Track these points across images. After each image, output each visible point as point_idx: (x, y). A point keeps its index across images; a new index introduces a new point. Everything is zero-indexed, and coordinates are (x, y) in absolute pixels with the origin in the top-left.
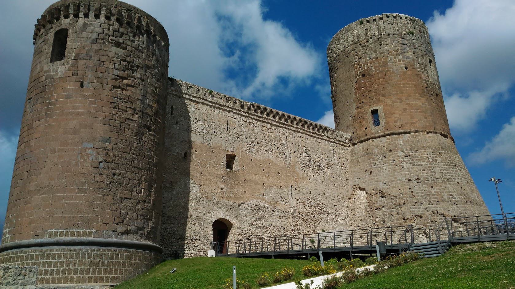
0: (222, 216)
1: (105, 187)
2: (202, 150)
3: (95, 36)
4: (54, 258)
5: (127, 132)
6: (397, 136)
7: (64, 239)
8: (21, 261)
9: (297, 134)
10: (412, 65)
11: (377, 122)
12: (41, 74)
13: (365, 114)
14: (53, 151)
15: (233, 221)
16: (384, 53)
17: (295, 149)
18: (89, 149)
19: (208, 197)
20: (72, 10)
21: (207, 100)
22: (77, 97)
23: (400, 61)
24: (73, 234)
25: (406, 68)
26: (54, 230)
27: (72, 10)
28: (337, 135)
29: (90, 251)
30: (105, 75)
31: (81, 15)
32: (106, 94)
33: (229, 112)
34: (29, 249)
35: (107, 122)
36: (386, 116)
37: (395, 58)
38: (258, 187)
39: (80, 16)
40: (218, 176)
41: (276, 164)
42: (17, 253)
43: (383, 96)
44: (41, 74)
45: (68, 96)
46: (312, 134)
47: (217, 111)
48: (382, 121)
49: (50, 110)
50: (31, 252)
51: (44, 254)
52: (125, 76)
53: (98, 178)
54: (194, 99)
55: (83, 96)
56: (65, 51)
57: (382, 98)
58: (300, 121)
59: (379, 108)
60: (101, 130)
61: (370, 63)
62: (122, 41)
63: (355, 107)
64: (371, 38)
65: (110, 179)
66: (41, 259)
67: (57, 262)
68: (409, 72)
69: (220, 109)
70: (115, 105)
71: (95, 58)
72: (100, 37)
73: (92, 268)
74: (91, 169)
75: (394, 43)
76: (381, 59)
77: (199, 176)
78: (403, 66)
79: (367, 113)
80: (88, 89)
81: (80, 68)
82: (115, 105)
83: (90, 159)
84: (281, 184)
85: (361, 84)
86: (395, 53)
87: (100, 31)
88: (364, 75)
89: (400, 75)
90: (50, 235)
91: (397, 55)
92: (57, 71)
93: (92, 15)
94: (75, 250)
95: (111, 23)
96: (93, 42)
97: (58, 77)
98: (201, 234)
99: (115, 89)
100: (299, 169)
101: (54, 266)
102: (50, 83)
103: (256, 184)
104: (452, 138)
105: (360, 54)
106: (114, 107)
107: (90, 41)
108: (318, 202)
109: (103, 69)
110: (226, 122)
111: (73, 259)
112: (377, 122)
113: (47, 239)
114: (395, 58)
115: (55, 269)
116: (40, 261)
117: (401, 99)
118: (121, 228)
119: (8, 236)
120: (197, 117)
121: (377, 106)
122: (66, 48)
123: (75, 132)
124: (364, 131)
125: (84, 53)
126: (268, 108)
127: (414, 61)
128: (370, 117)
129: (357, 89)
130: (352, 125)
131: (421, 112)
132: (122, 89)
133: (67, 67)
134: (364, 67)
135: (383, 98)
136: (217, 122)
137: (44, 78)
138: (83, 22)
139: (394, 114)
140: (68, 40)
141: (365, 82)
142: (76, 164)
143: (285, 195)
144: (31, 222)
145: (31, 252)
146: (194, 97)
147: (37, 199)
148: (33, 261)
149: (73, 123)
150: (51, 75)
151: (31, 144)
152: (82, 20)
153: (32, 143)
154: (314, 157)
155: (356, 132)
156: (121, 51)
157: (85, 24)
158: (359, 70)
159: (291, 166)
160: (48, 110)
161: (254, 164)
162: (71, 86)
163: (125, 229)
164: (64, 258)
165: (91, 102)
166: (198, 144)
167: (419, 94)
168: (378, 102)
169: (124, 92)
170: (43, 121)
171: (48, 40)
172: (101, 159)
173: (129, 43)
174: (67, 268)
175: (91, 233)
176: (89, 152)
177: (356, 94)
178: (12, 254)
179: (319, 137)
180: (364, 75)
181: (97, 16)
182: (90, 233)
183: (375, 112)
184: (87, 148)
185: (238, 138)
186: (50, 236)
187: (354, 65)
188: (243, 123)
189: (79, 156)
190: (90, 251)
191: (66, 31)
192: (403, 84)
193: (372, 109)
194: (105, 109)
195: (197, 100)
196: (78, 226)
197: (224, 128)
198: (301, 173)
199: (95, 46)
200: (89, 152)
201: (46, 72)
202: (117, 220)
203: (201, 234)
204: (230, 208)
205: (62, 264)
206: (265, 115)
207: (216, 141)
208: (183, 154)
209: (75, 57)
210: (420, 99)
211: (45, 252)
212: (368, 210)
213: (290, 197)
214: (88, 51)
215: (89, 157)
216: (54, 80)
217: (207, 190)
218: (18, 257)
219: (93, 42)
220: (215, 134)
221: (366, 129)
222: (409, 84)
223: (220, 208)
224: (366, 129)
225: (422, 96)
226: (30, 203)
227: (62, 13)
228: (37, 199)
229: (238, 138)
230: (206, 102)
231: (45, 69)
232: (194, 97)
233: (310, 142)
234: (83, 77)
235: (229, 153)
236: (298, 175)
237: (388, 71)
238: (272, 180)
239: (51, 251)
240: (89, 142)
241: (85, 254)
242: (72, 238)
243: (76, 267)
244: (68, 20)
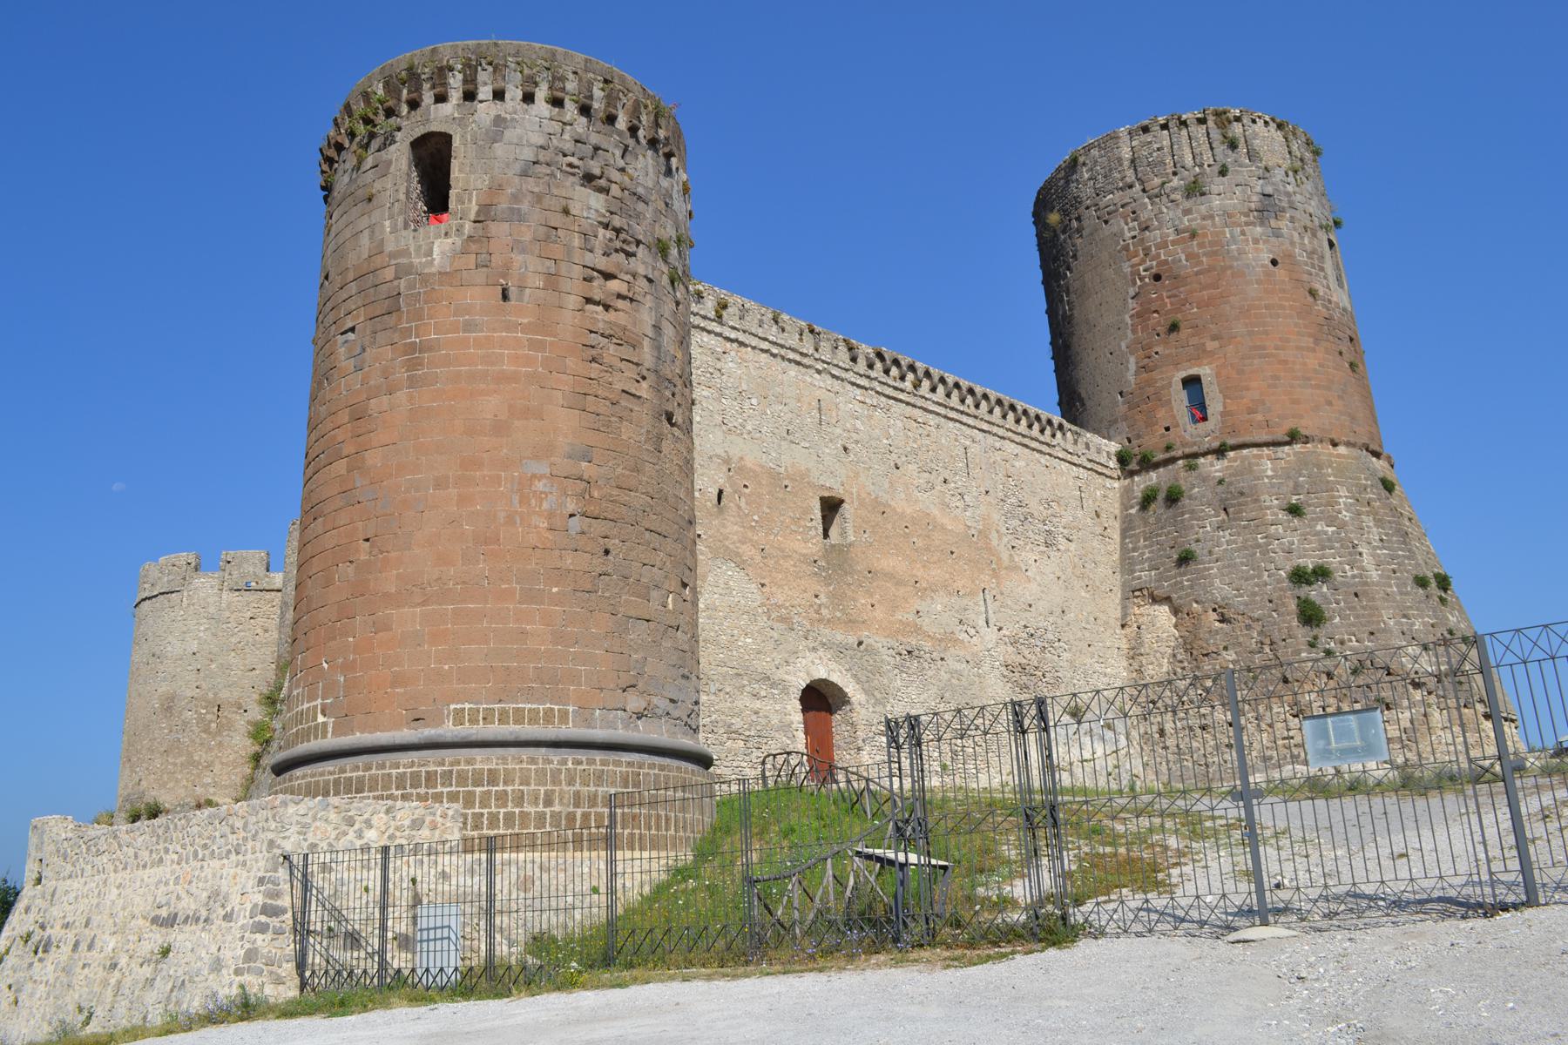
0: (821, 673)
1: (588, 587)
2: (760, 483)
3: (528, 154)
4: (478, 782)
5: (627, 432)
6: (1255, 451)
7: (495, 730)
8: (385, 788)
9: (991, 439)
10: (1290, 256)
11: (1199, 410)
12: (378, 261)
13: (1163, 388)
14: (440, 484)
15: (850, 688)
16: (1212, 217)
17: (988, 485)
18: (540, 478)
19: (782, 619)
20: (456, 82)
21: (765, 339)
22: (494, 330)
23: (1256, 241)
24: (519, 717)
25: (1274, 262)
26: (467, 706)
27: (456, 82)
28: (1088, 447)
29: (570, 765)
30: (563, 267)
31: (485, 92)
32: (570, 315)
33: (819, 372)
34: (404, 758)
35: (579, 400)
36: (1225, 397)
37: (1243, 233)
38: (902, 590)
39: (481, 96)
40: (804, 559)
41: (943, 528)
42: (368, 768)
43: (1215, 338)
44: (378, 261)
45: (469, 327)
46: (1026, 441)
47: (793, 371)
48: (1214, 406)
49: (421, 364)
50: (412, 764)
51: (451, 772)
52: (611, 270)
53: (569, 561)
54: (733, 335)
55: (510, 327)
56: (447, 197)
57: (1211, 345)
58: (999, 402)
59: (1205, 371)
60: (565, 426)
61: (1174, 243)
62: (597, 172)
63: (1132, 366)
64: (1175, 174)
65: (598, 564)
66: (443, 785)
67: (489, 792)
68: (1280, 272)
69: (798, 363)
70: (594, 352)
71: (536, 216)
72: (541, 158)
73: (579, 812)
74: (549, 535)
75: (1238, 190)
76: (1205, 235)
77: (758, 558)
78: (1266, 258)
79: (1170, 384)
80: (523, 311)
81: (494, 246)
82: (594, 352)
83: (545, 505)
84: (959, 585)
85: (1151, 301)
86: (1243, 219)
87: (539, 140)
88: (1157, 278)
89: (1259, 282)
90: (459, 717)
91: (1247, 224)
92: (430, 253)
93: (514, 93)
94: (533, 761)
95: (568, 118)
96: (524, 174)
97: (434, 270)
98: (775, 721)
99: (590, 307)
100: (1000, 544)
101: (483, 805)
102: (411, 286)
103: (900, 583)
104: (1389, 459)
105: (1144, 216)
106: (594, 360)
107: (518, 167)
108: (1050, 636)
109: (557, 251)
110: (815, 403)
111: (528, 784)
112: (1199, 410)
113: (449, 730)
114: (1243, 233)
115: (485, 811)
116: (439, 789)
117: (1264, 348)
118: (635, 702)
119: (321, 719)
120: (744, 387)
121: (1199, 366)
122: (449, 187)
123: (500, 428)
124: (1162, 436)
125: (503, 205)
126: (918, 364)
127: (1292, 243)
128: (1180, 398)
129: (1138, 315)
130: (1125, 418)
131: (1317, 387)
132: (607, 307)
133: (459, 241)
134: (1158, 255)
135: (1216, 344)
136: (793, 404)
137: (389, 274)
138: (493, 113)
139: (1248, 389)
140: (455, 165)
141: (1161, 296)
142: (510, 520)
143: (971, 615)
144: (397, 681)
145: (412, 764)
146: (734, 328)
147: (407, 618)
148: (422, 791)
149: (491, 406)
150: (411, 265)
151: (369, 462)
152: (486, 110)
153: (373, 458)
154: (1035, 507)
155: (1139, 437)
156: (597, 202)
157: (498, 120)
158: (1143, 262)
159: (980, 532)
160: (413, 365)
161: (889, 526)
162: (478, 296)
163: (644, 705)
164: (505, 783)
165: (536, 346)
166: (749, 465)
167: (1310, 335)
168: (1200, 354)
169: (611, 316)
170: (401, 396)
171: (389, 163)
172: (571, 507)
173: (616, 176)
174: (517, 811)
175: (567, 712)
176: (539, 486)
177: (1134, 331)
178: (353, 770)
179: (1044, 448)
180: (1157, 278)
181: (528, 98)
182: (564, 716)
183: (1192, 383)
184: (534, 476)
185: (845, 449)
186: (459, 721)
187: (1126, 248)
188: (858, 407)
189: (516, 499)
190: (570, 765)
191: (446, 139)
192: (1266, 307)
193: (1184, 374)
194: (572, 363)
195: (742, 337)
196: (530, 695)
197: (810, 420)
198: (1005, 556)
199: (530, 184)
200: (539, 486)
201: (392, 255)
202: (625, 680)
203: (775, 721)
204: (840, 651)
205: (502, 798)
206: (908, 385)
207: (794, 458)
208: (716, 493)
209: (478, 213)
210: (1314, 350)
211: (452, 764)
212: (1179, 657)
213: (982, 622)
214: (515, 198)
215: (541, 500)
216: (425, 279)
217: (779, 598)
218: (374, 779)
219: (524, 174)
220: (790, 437)
221: (1167, 429)
222: (1282, 307)
223: (814, 649)
224: (1167, 429)
225: (1317, 341)
226: (388, 628)
227: (426, 86)
228: (407, 618)
229: (845, 449)
230: (765, 345)
231: (390, 247)
232: (734, 328)
233: (1023, 463)
234: (505, 271)
235: (826, 494)
236: (1000, 559)
237: (1224, 269)
238: (937, 574)
239: (468, 762)
240: (536, 457)
241: (559, 771)
242: (611, 731)
243: (541, 808)
244: (447, 109)
